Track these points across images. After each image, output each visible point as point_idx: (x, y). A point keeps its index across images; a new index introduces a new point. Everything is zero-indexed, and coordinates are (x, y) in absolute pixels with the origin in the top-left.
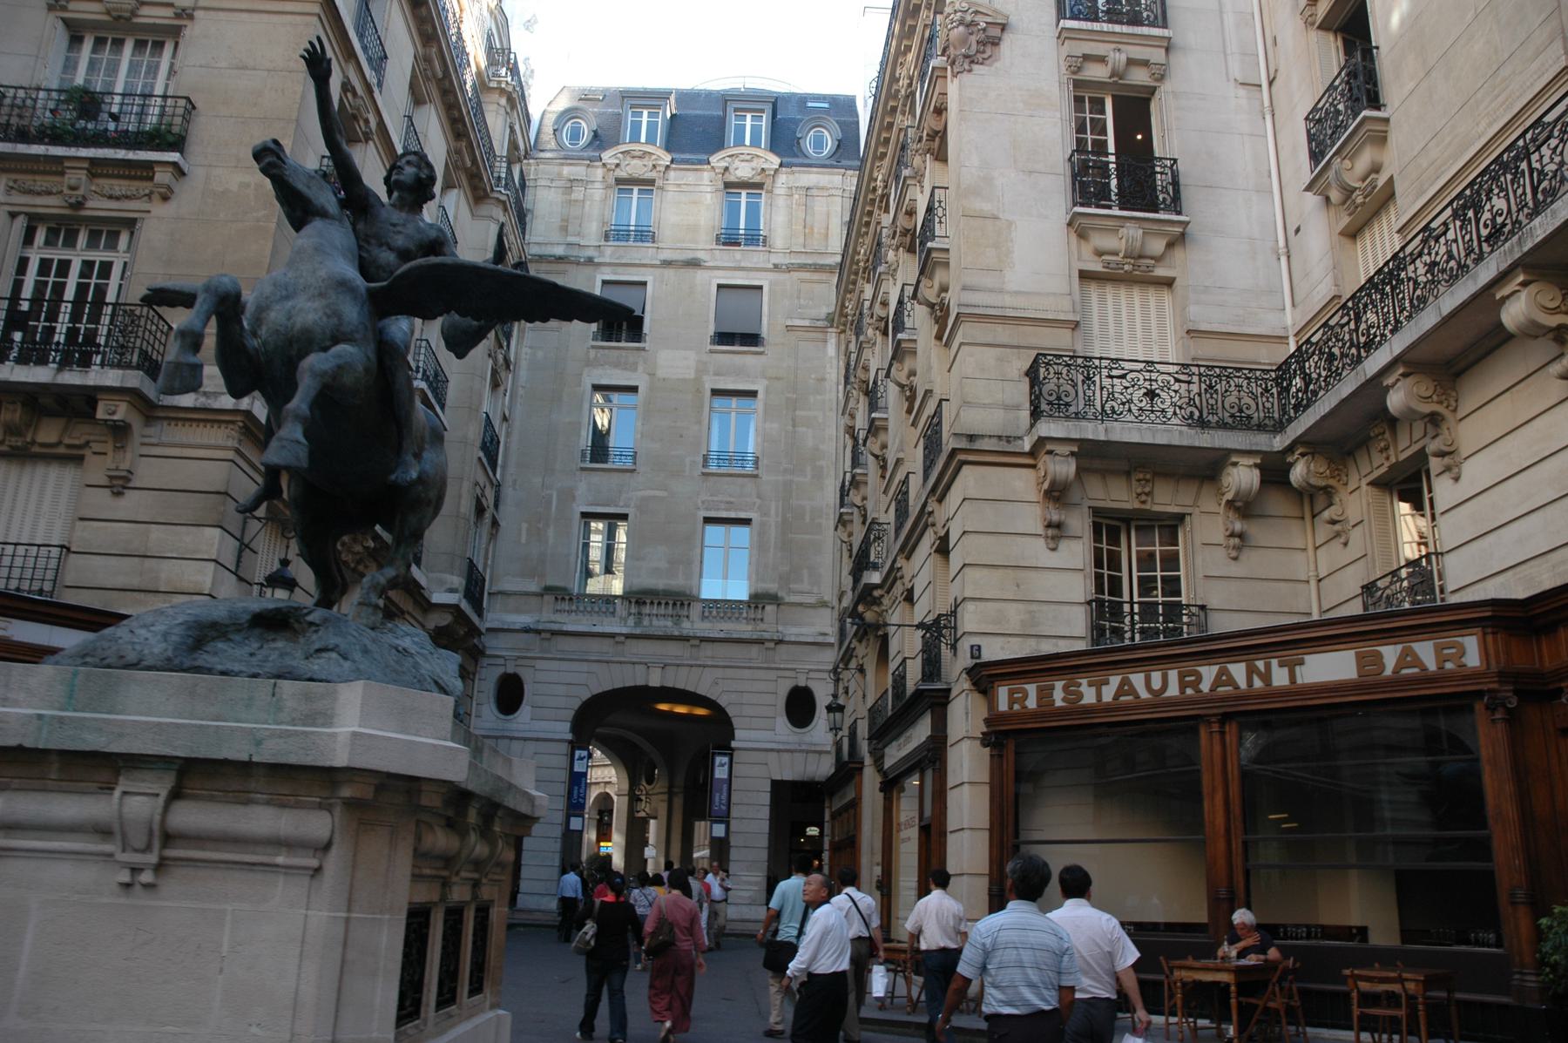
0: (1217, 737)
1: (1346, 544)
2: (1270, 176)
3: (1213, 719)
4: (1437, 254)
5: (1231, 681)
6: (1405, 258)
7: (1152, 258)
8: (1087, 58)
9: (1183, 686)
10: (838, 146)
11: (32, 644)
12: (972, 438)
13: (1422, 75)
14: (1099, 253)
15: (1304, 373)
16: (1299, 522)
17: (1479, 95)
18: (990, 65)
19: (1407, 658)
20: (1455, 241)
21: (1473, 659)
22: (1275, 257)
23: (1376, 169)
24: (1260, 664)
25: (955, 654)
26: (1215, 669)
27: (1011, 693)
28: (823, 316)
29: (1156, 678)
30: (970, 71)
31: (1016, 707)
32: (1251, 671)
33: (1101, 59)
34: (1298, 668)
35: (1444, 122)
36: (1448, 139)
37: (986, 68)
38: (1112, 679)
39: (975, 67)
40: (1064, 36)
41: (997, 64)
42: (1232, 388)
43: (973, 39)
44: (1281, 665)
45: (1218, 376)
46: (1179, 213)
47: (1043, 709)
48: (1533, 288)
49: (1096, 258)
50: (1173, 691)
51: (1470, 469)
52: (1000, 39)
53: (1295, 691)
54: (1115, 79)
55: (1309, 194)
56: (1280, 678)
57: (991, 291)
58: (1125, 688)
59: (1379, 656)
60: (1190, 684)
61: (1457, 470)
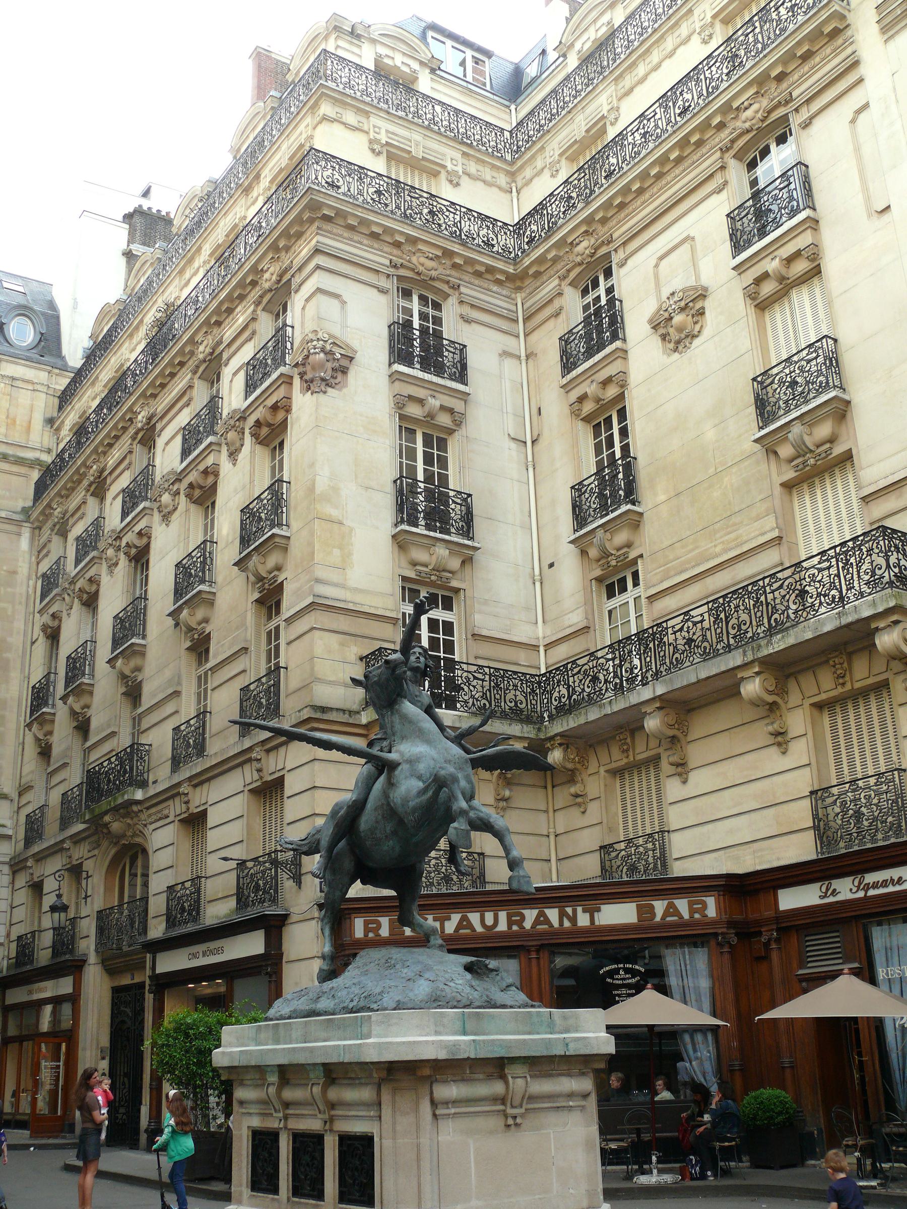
0: (534, 962)
1: (583, 813)
2: (530, 516)
3: (533, 949)
4: (694, 634)
5: (547, 921)
6: (667, 628)
7: (450, 572)
8: (410, 397)
9: (510, 923)
10: (40, 340)
11: (175, 951)
12: (324, 709)
13: (673, 494)
14: (414, 564)
15: (569, 686)
16: (543, 791)
17: (717, 526)
18: (340, 390)
19: (671, 910)
20: (709, 629)
21: (712, 912)
22: (531, 581)
23: (629, 545)
24: (569, 910)
25: (300, 888)
26: (535, 912)
27: (366, 923)
28: (19, 509)
29: (489, 918)
30: (325, 392)
31: (371, 935)
32: (562, 914)
33: (421, 402)
34: (596, 914)
35: (688, 533)
36: (691, 547)
37: (337, 392)
38: (453, 916)
39: (329, 390)
40: (394, 377)
41: (345, 390)
42: (511, 687)
43: (329, 365)
44: (584, 911)
45: (502, 677)
46: (472, 539)
47: (395, 937)
48: (763, 676)
49: (410, 567)
50: (502, 926)
51: (693, 777)
52: (348, 368)
53: (593, 930)
54: (429, 419)
55: (572, 546)
56: (583, 920)
57: (336, 585)
58: (464, 923)
59: (653, 907)
60: (372, 930)
61: (685, 776)
